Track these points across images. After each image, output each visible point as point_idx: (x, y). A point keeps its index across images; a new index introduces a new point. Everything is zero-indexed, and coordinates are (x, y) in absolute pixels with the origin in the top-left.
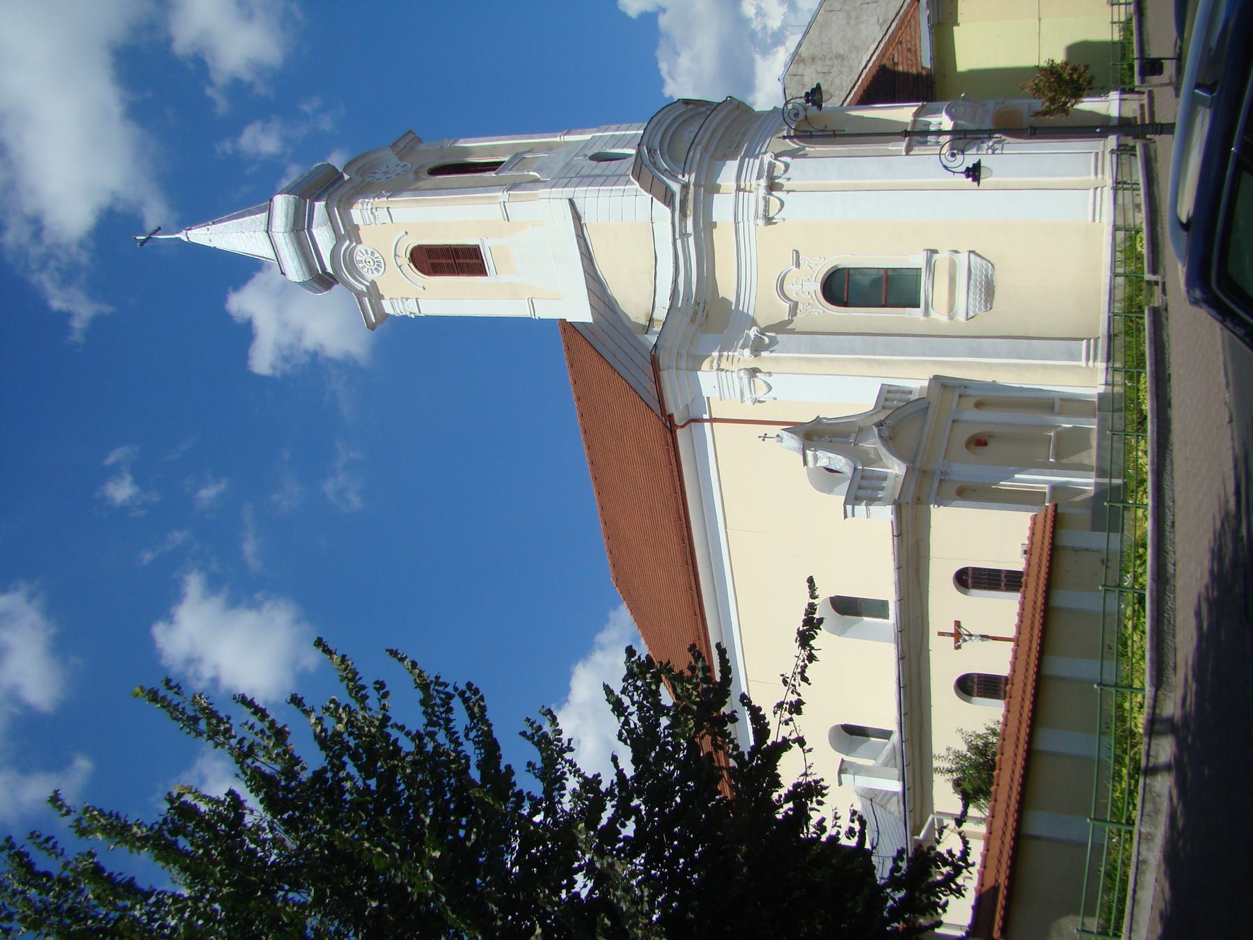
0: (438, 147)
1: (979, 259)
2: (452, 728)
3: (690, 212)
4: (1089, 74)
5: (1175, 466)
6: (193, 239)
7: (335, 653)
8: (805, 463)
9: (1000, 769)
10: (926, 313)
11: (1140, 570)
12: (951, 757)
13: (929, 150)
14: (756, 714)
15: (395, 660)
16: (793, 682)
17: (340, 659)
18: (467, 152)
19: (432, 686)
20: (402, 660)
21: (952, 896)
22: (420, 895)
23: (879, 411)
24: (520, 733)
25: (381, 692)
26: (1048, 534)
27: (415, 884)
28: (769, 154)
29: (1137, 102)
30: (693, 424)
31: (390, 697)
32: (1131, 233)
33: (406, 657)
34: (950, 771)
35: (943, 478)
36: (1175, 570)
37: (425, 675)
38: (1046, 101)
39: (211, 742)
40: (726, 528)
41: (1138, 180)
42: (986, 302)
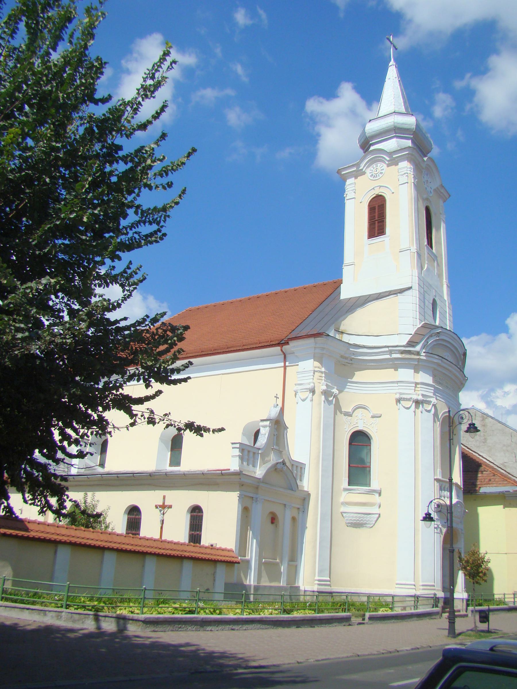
0: (441, 212)
1: (375, 519)
2: (140, 225)
3: (403, 356)
4: (482, 582)
5: (265, 630)
6: (390, 69)
7: (187, 159)
8: (262, 421)
9: (93, 532)
10: (345, 490)
11: (207, 611)
12: (93, 503)
15: (180, 193)
16: (166, 419)
17: (184, 162)
18: (438, 229)
19: (164, 213)
23: (291, 463)
25: (166, 186)
26: (223, 558)
27: (67, 206)
28: (436, 401)
29: (462, 608)
30: (283, 356)
31: (163, 190)
32: (391, 605)
33: (181, 199)
34: (85, 502)
35: (254, 499)
36: (208, 631)
37: (171, 210)
38: (467, 559)
40: (223, 374)
41: (419, 609)
42: (351, 523)
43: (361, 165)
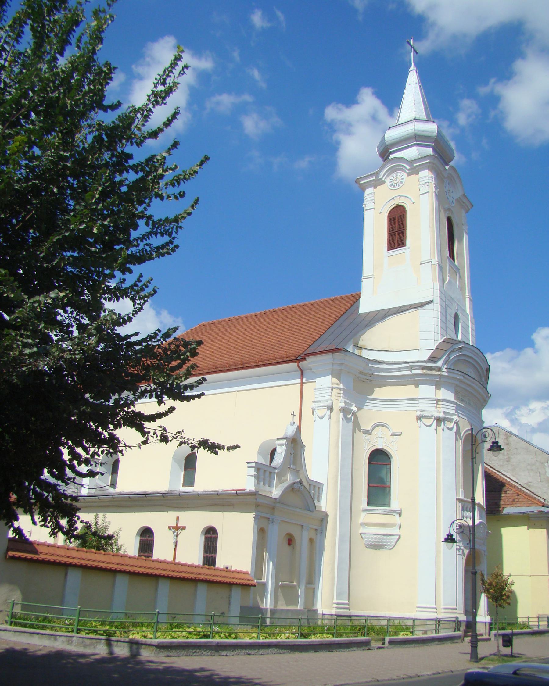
0: (464, 223)
1: (396, 540)
2: (151, 236)
3: (425, 372)
4: (505, 605)
7: (200, 168)
8: (279, 439)
10: (364, 510)
13: (459, 513)
14: (160, 415)
15: (192, 203)
16: (179, 437)
17: (196, 170)
18: (460, 240)
20: (193, 206)
21: (50, 530)
22: (68, 220)
23: (308, 482)
24: (141, 274)
25: (178, 196)
26: (239, 581)
28: (458, 418)
30: (300, 372)
33: (194, 209)
34: (96, 524)
35: (270, 519)
36: (223, 655)
37: (183, 221)
38: (490, 581)
39: (150, 93)
40: (237, 391)
41: (441, 633)
43: (380, 174)
